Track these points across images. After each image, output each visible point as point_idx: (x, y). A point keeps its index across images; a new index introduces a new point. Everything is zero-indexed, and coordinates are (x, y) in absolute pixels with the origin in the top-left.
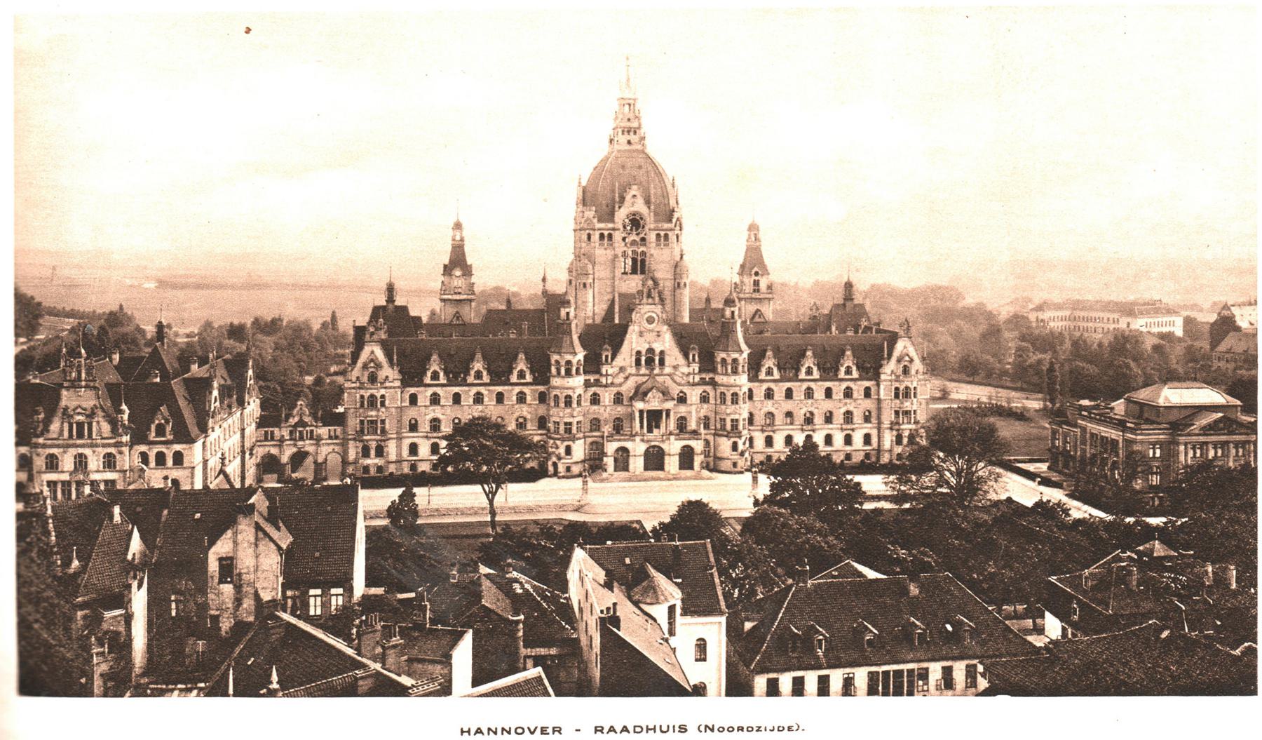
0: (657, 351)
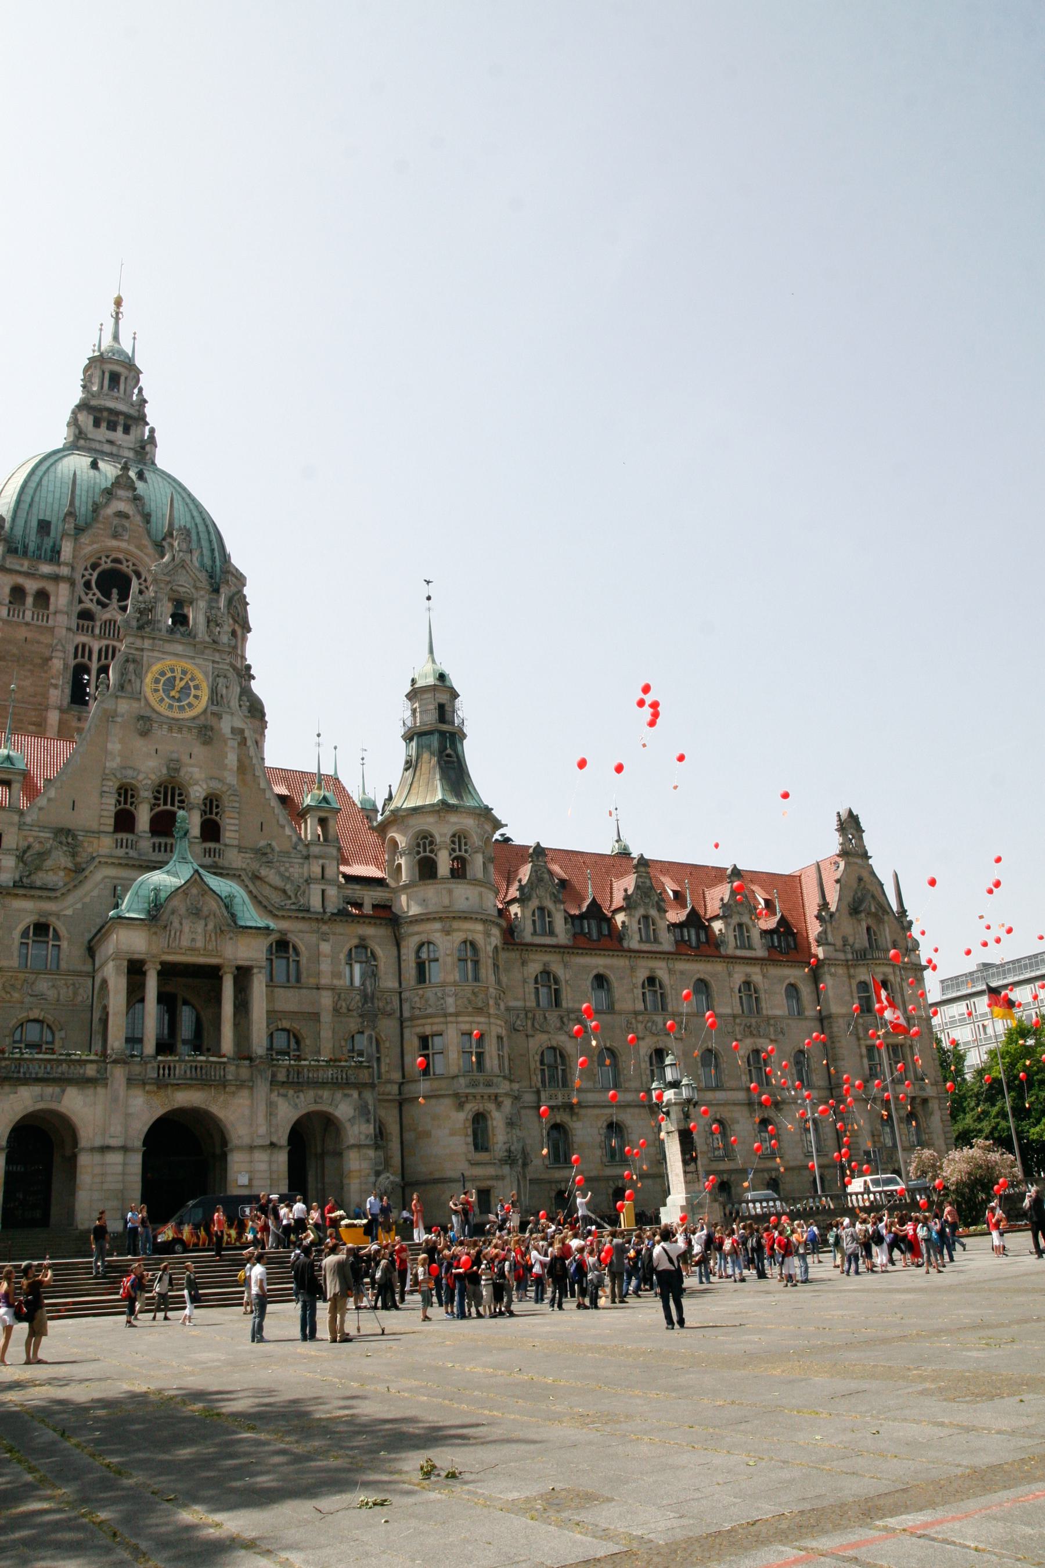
0: (197, 793)
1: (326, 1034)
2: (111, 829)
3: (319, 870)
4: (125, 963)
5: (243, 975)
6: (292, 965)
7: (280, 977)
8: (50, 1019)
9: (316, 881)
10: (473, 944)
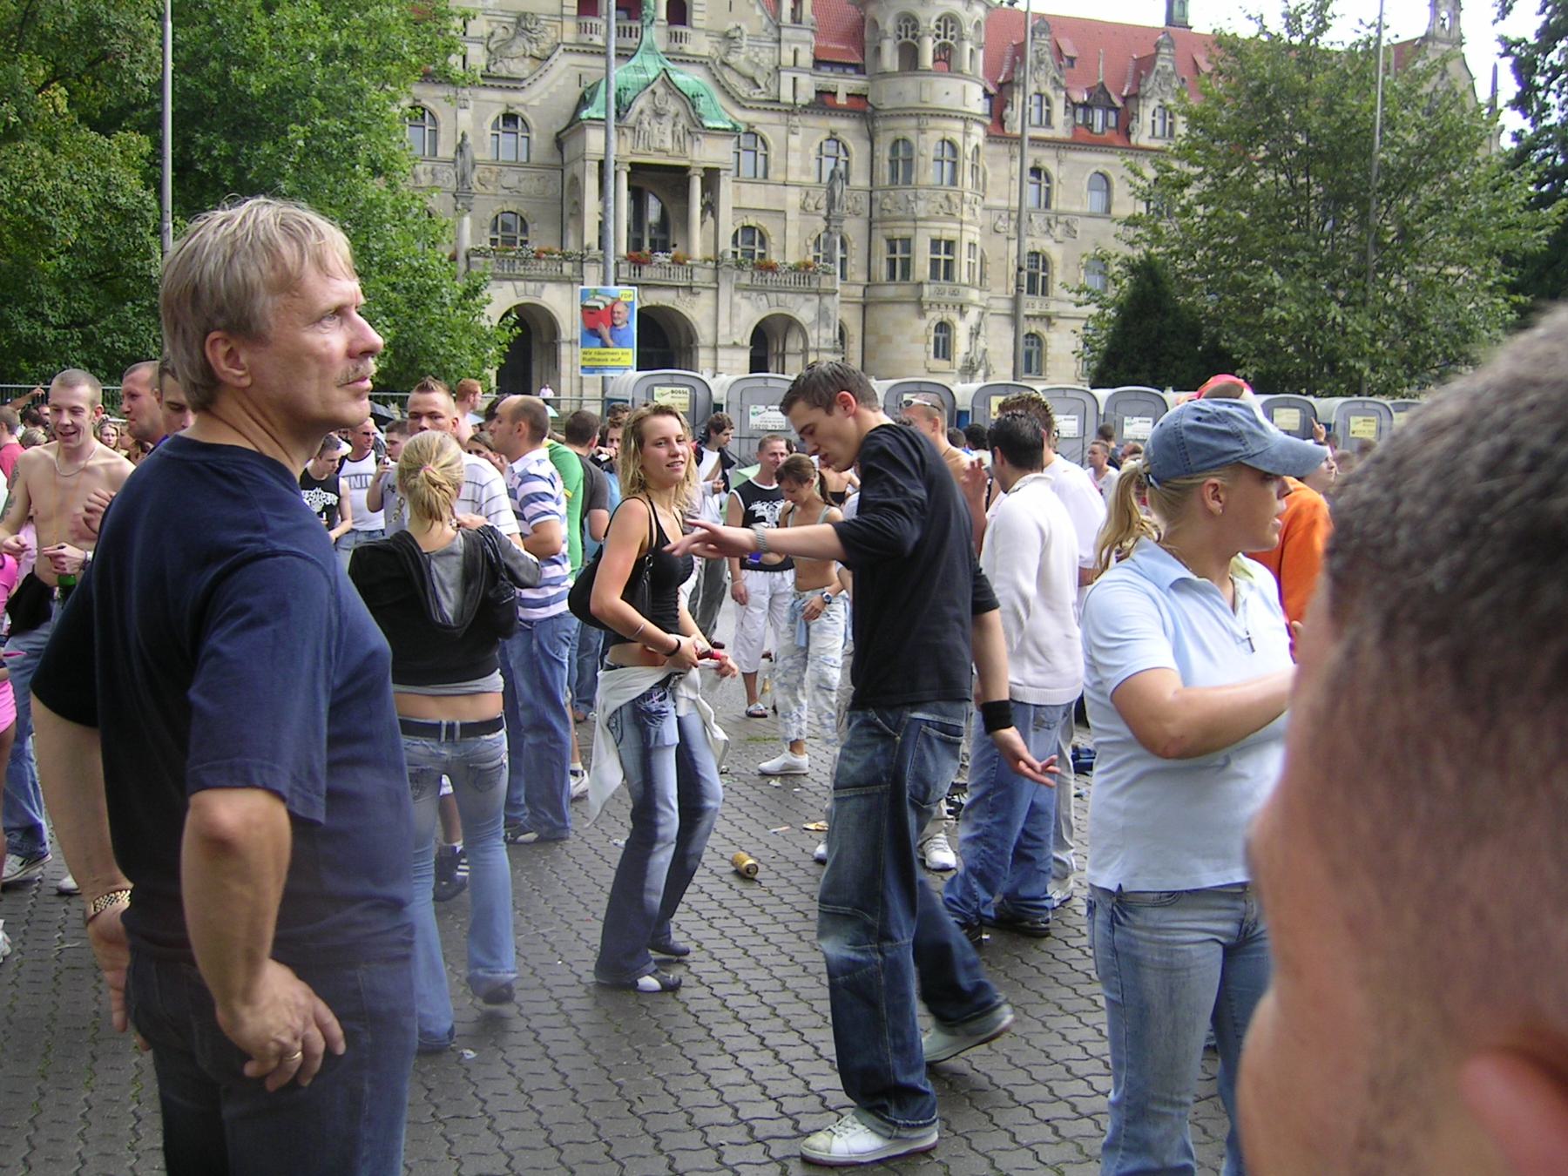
1: (792, 232)
2: (575, 12)
3: (791, 55)
5: (711, 177)
6: (760, 159)
7: (747, 170)
9: (788, 69)
10: (952, 144)
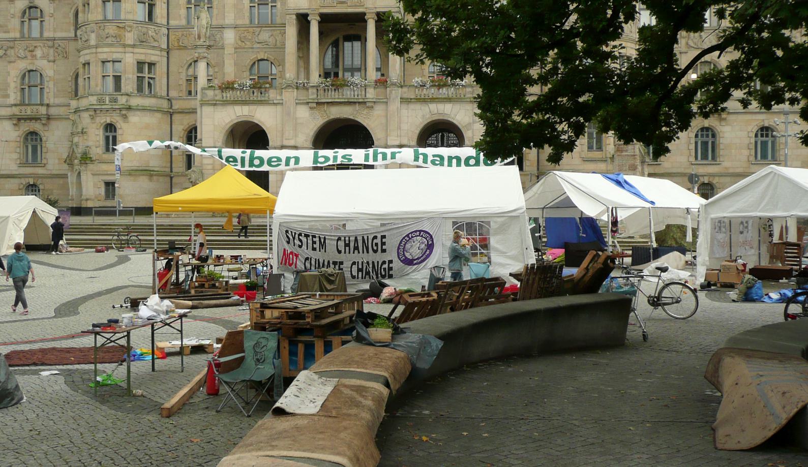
4: (294, 17)
8: (272, 58)
